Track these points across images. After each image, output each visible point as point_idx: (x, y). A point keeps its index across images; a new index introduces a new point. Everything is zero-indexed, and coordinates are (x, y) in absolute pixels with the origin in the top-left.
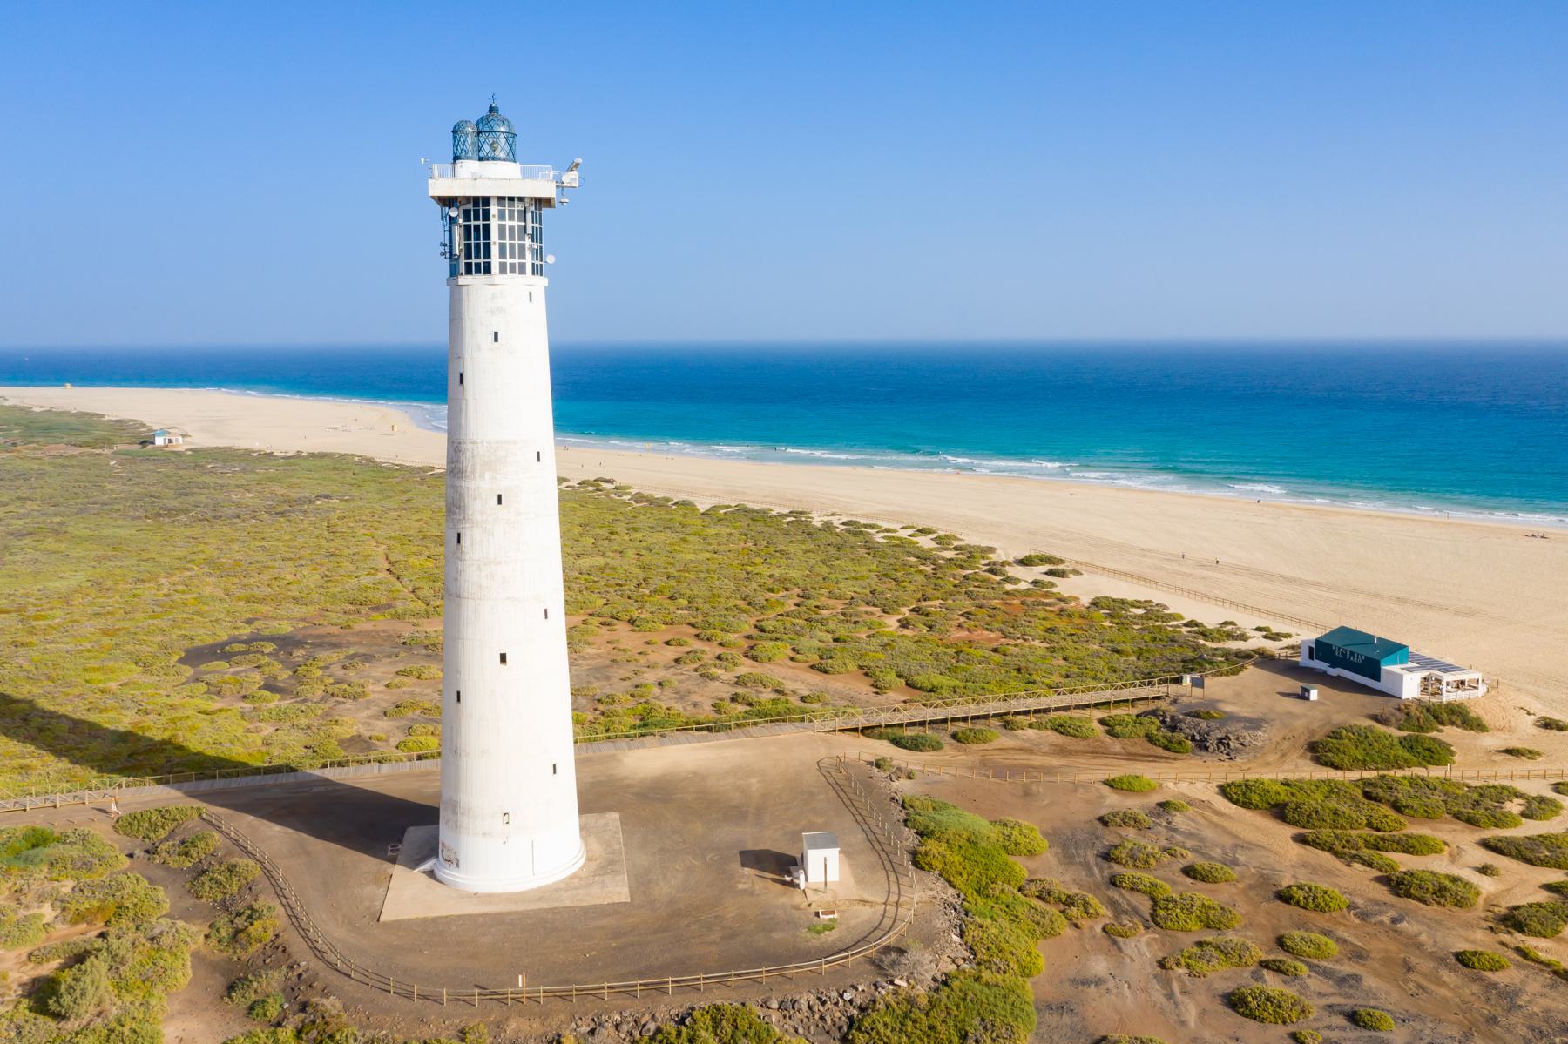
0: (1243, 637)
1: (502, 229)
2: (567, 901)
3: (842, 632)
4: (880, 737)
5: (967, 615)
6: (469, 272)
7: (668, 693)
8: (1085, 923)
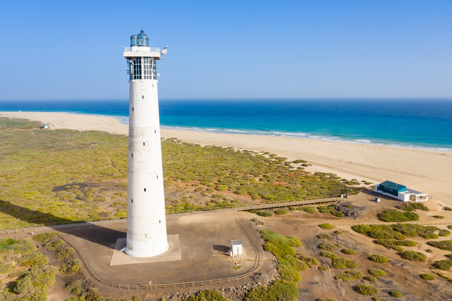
0: (358, 184)
1: (145, 66)
2: (163, 260)
3: (243, 182)
4: (254, 212)
5: (279, 177)
6: (135, 78)
7: (193, 200)
8: (313, 266)
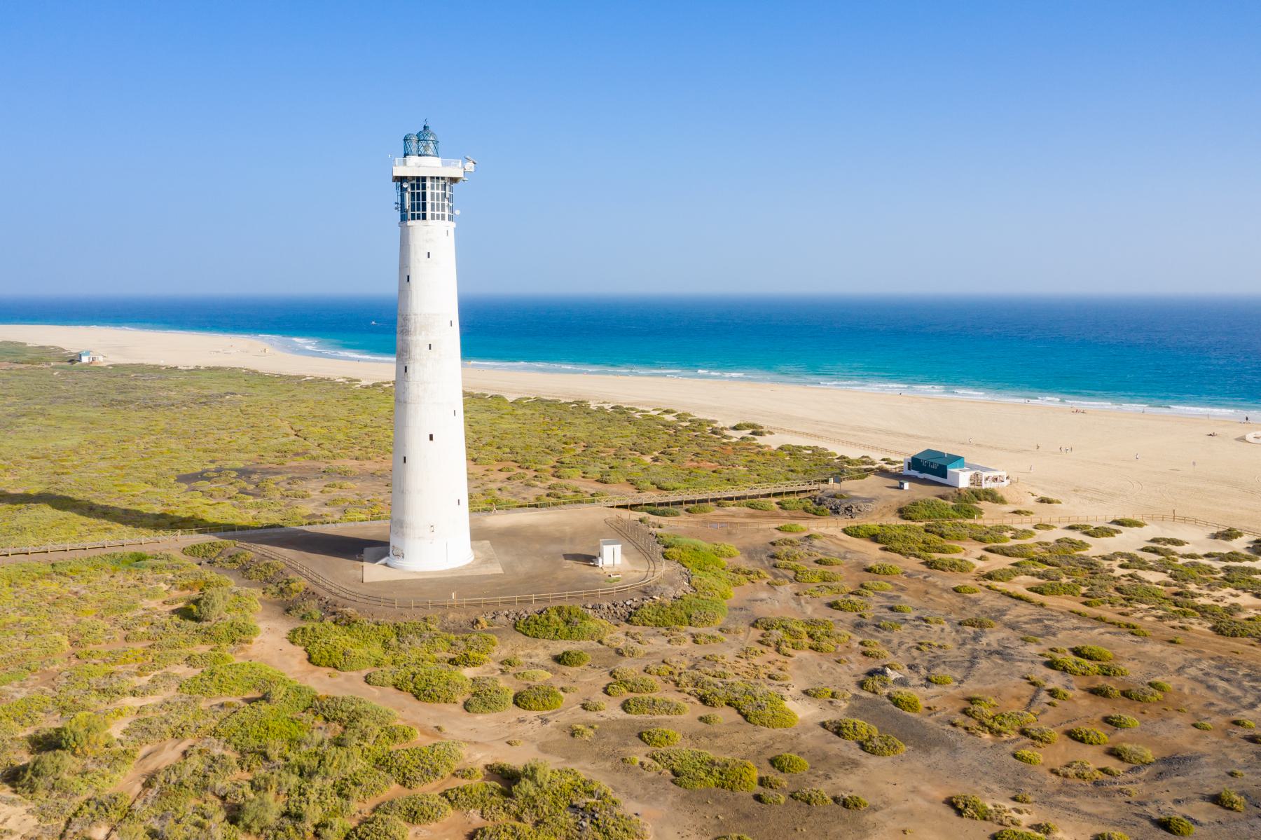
0: (873, 463)
1: (432, 194)
2: (468, 573)
3: (614, 463)
4: (642, 510)
5: (697, 454)
6: (413, 218)
7: (505, 493)
8: (758, 581)
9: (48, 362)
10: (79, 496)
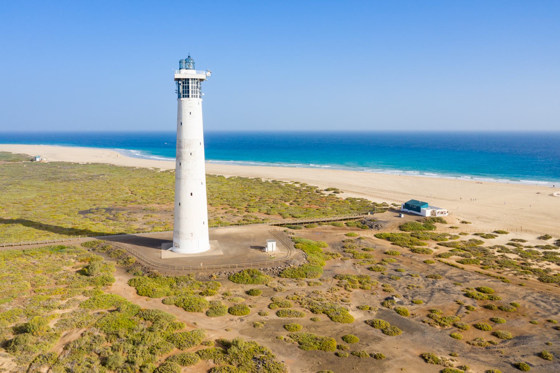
0: (388, 206)
1: (192, 86)
2: (208, 255)
3: (273, 206)
4: (285, 227)
5: (309, 202)
6: (183, 97)
7: (224, 219)
8: (336, 258)
9: (21, 161)
10: (35, 220)
